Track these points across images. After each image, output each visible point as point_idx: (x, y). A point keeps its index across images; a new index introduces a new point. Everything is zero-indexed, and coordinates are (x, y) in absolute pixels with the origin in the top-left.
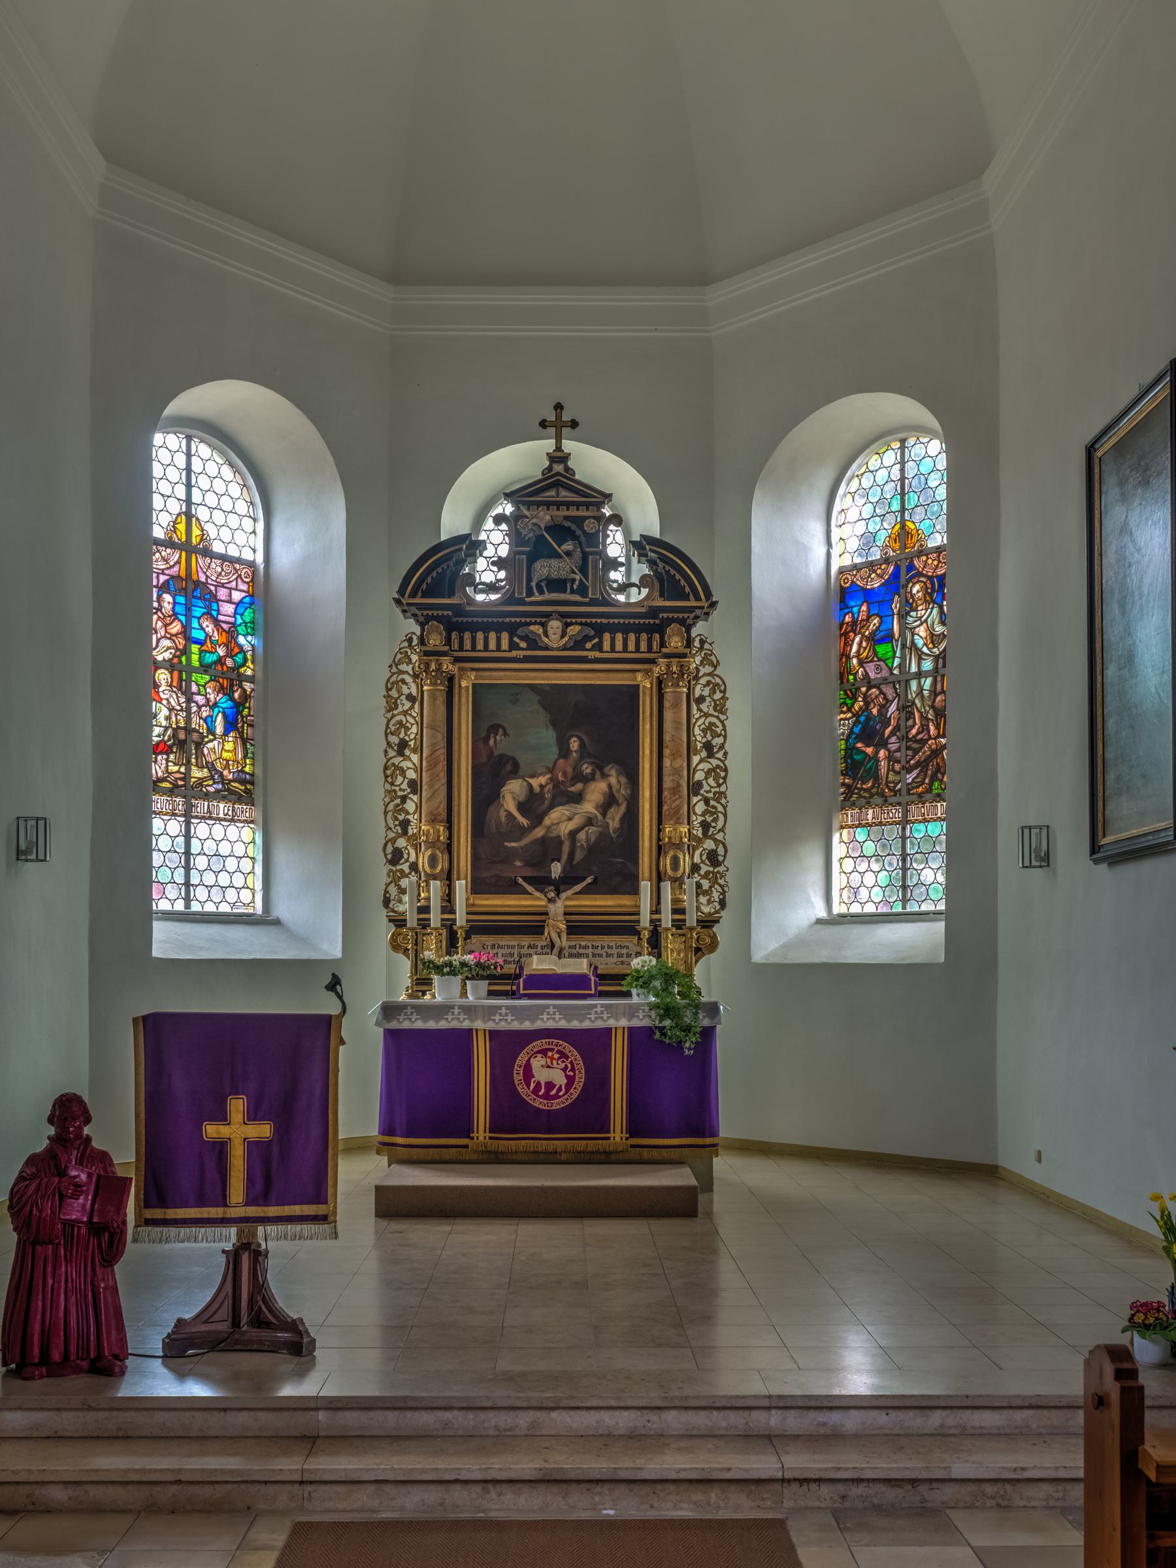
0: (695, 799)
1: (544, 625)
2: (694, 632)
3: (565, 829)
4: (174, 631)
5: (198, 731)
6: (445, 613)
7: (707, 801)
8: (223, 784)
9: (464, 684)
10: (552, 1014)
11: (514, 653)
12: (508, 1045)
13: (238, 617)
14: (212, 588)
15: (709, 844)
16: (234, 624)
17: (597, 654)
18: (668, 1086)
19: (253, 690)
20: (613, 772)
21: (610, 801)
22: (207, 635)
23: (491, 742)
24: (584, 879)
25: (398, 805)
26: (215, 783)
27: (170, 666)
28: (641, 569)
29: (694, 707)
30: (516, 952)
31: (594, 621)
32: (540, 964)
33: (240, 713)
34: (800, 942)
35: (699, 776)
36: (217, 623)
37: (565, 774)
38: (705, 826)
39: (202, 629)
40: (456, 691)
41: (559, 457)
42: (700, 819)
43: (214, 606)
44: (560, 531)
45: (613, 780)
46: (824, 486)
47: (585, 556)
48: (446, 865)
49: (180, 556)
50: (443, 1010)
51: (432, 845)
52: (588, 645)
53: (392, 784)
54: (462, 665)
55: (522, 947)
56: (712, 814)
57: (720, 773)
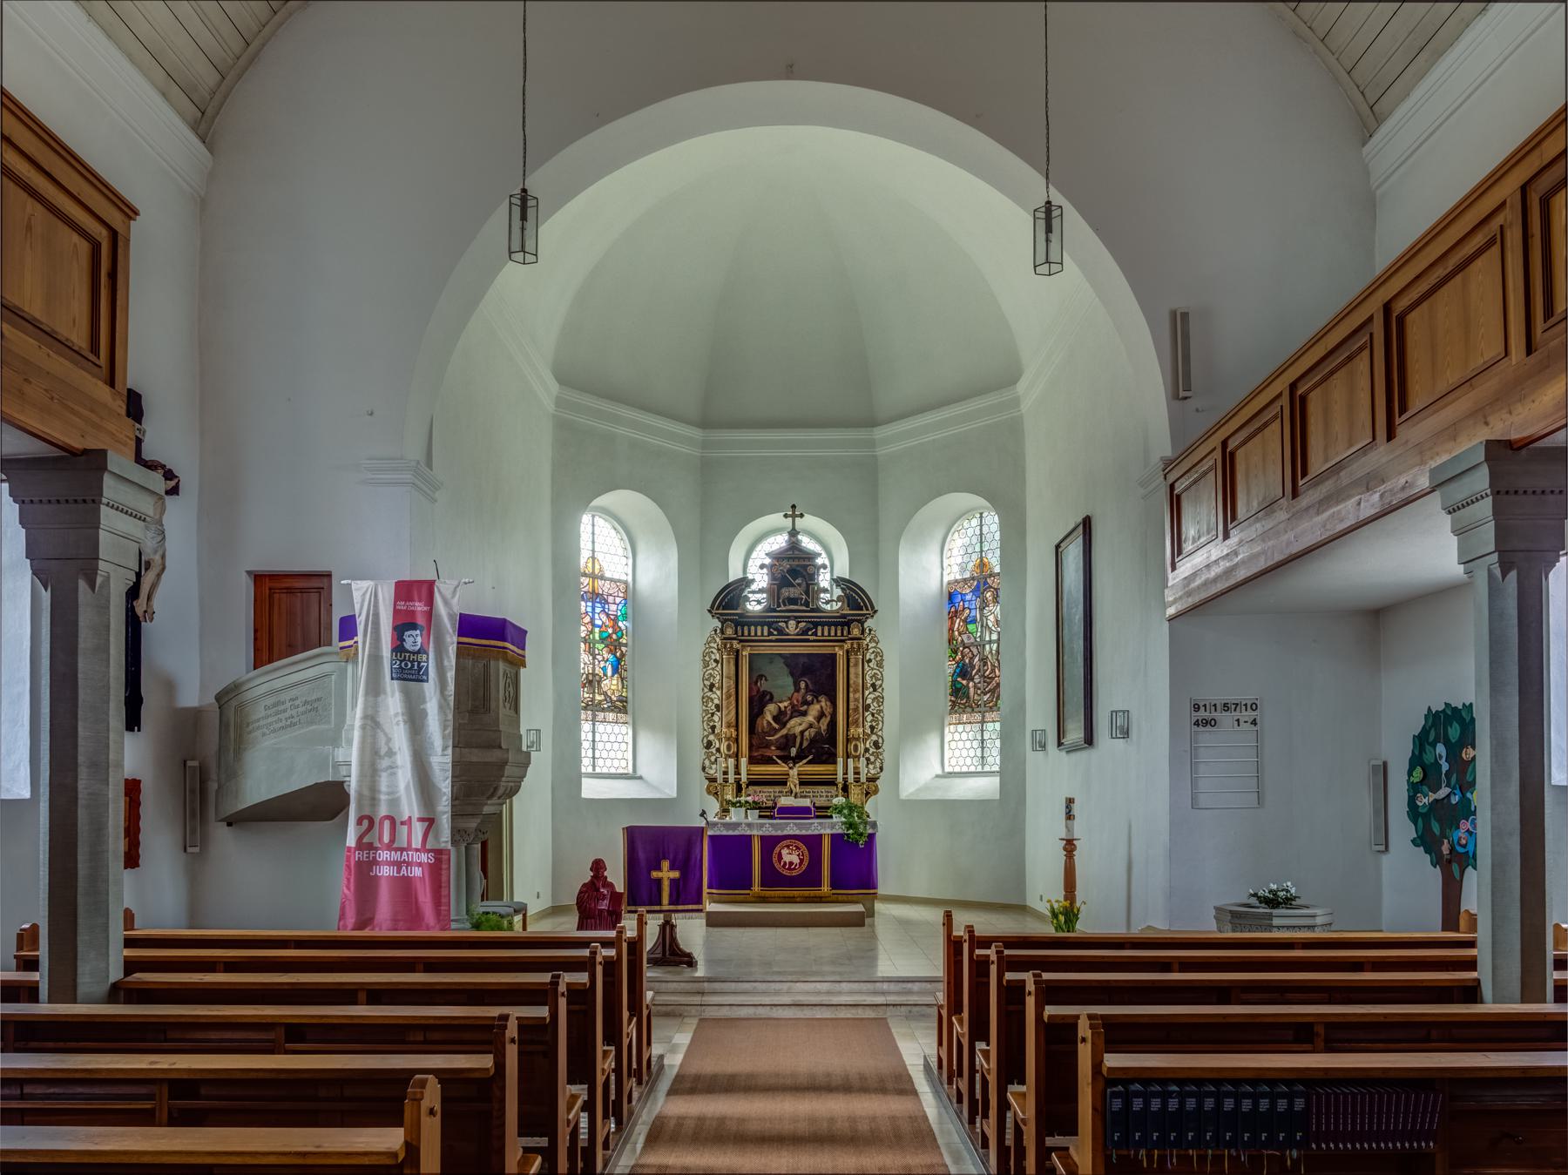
3: (798, 729)
10: (792, 827)
12: (769, 843)
15: (874, 738)
18: (852, 865)
27: (585, 641)
28: (838, 592)
32: (785, 801)
34: (926, 788)
36: (608, 615)
38: (872, 728)
44: (794, 572)
46: (939, 536)
47: (808, 586)
50: (736, 825)
51: (728, 739)
57: (880, 700)
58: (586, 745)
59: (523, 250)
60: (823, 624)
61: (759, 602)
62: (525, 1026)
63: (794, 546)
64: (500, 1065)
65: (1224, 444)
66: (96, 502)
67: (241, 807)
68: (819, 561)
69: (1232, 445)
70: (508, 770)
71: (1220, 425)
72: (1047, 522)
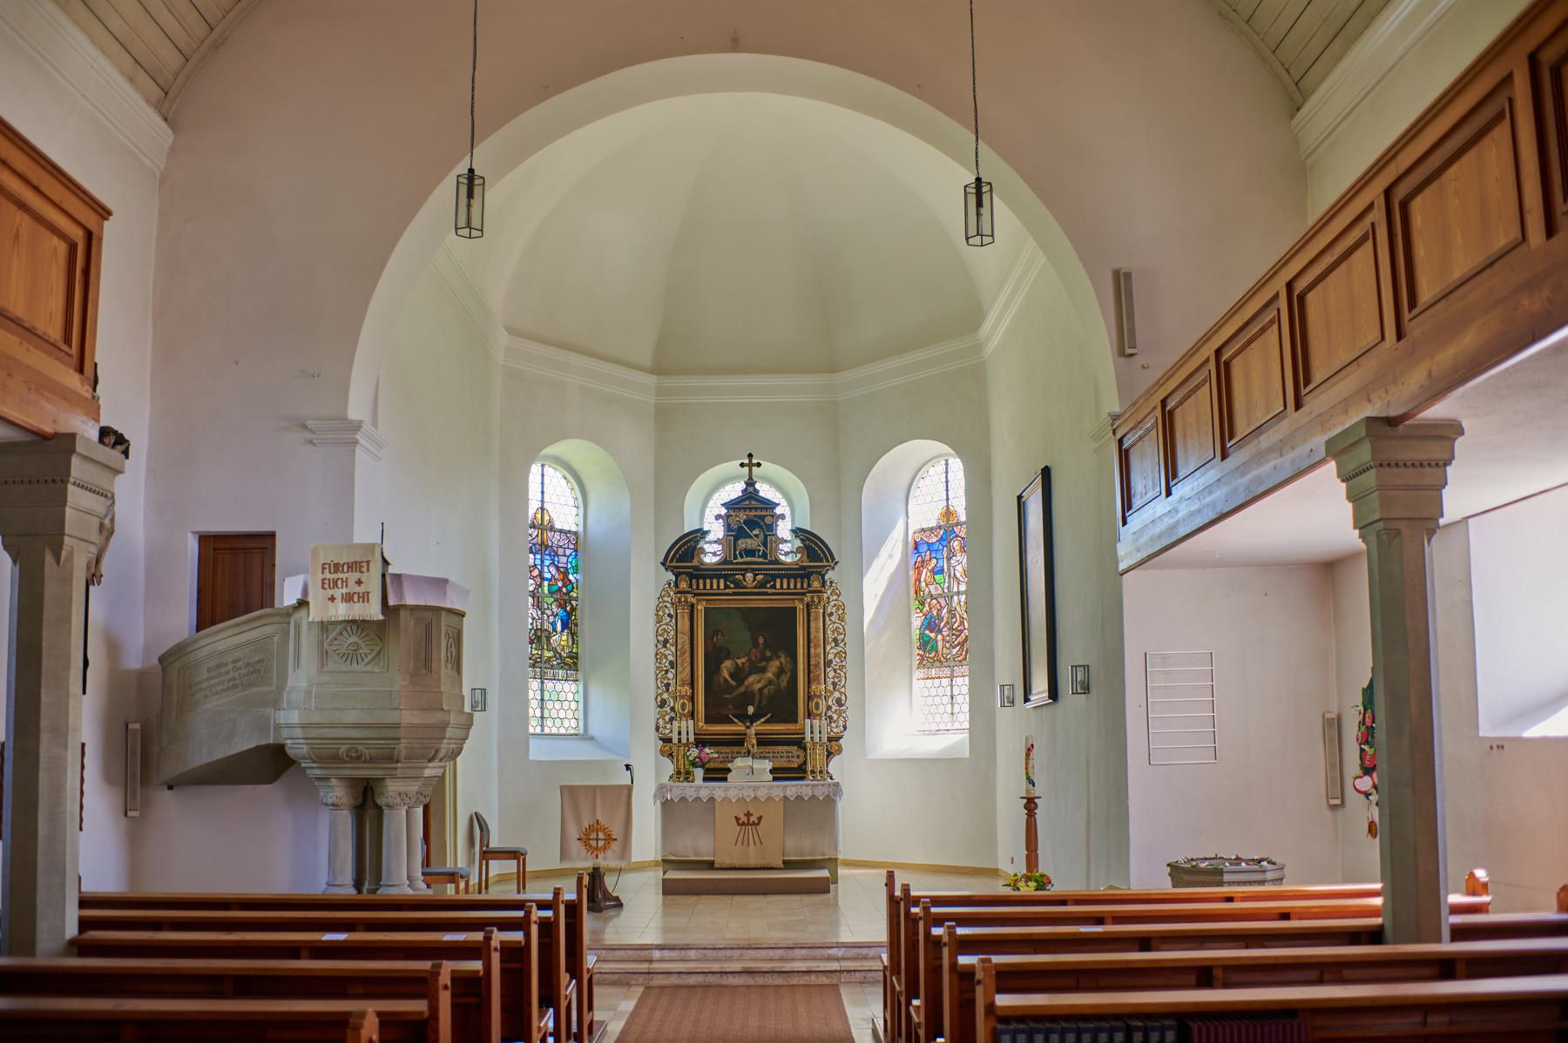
3: (757, 686)
15: (837, 694)
21: (781, 672)
28: (798, 543)
35: (830, 657)
36: (557, 568)
38: (834, 684)
57: (842, 655)
58: (534, 704)
59: (469, 226)
60: (781, 577)
61: (714, 554)
62: (459, 979)
63: (750, 494)
64: (434, 1009)
65: (1164, 402)
66: (65, 482)
67: (181, 770)
68: (778, 511)
69: (1171, 405)
70: (449, 732)
71: (1160, 384)
72: (1012, 474)
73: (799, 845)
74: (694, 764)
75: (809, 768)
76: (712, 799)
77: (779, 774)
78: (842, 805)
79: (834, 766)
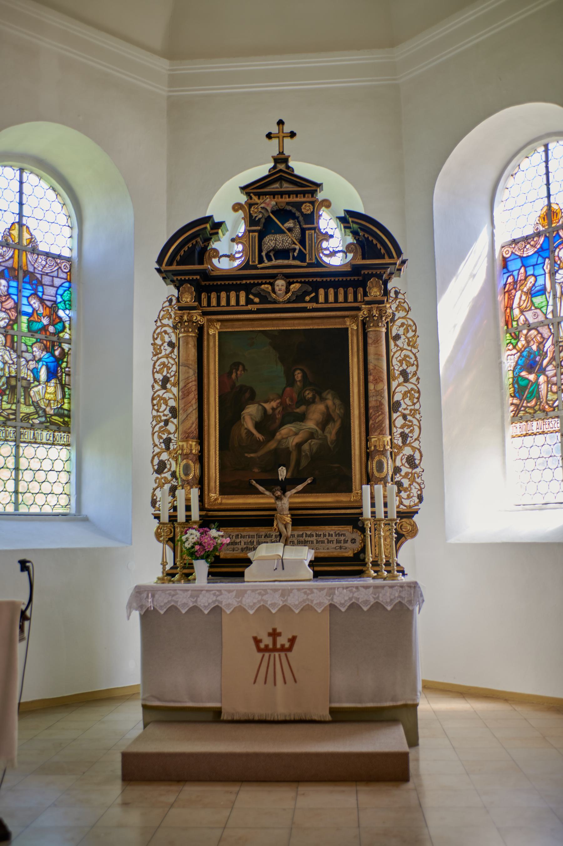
0: (395, 416)
1: (272, 284)
2: (390, 286)
3: (294, 441)
4: (8, 307)
5: (26, 379)
6: (195, 277)
7: (405, 417)
8: (46, 418)
9: (211, 332)
11: (250, 307)
13: (59, 297)
14: (39, 276)
15: (407, 451)
16: (55, 302)
17: (315, 305)
19: (70, 349)
20: (329, 396)
21: (327, 419)
22: (34, 309)
23: (234, 376)
24: (305, 480)
25: (161, 427)
26: (39, 417)
29: (392, 343)
30: (255, 540)
31: (311, 280)
33: (60, 366)
35: (398, 397)
36: (42, 300)
37: (291, 399)
38: (404, 436)
39: (30, 305)
40: (205, 337)
41: (281, 159)
42: (400, 431)
43: (40, 289)
44: (283, 214)
45: (330, 403)
47: (303, 231)
48: (198, 472)
49: (13, 253)
52: (307, 298)
53: (158, 411)
54: (210, 317)
55: (260, 536)
56: (409, 426)
57: (414, 395)
60: (326, 286)
61: (231, 257)
73: (354, 685)
74: (193, 554)
75: (370, 558)
76: (217, 610)
77: (323, 567)
78: (423, 620)
79: (405, 555)
